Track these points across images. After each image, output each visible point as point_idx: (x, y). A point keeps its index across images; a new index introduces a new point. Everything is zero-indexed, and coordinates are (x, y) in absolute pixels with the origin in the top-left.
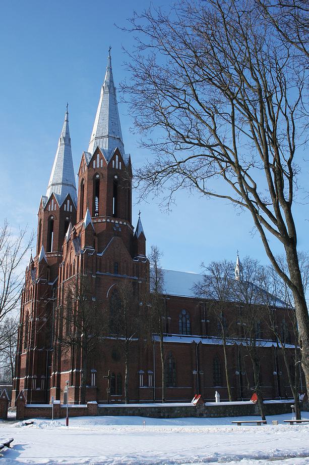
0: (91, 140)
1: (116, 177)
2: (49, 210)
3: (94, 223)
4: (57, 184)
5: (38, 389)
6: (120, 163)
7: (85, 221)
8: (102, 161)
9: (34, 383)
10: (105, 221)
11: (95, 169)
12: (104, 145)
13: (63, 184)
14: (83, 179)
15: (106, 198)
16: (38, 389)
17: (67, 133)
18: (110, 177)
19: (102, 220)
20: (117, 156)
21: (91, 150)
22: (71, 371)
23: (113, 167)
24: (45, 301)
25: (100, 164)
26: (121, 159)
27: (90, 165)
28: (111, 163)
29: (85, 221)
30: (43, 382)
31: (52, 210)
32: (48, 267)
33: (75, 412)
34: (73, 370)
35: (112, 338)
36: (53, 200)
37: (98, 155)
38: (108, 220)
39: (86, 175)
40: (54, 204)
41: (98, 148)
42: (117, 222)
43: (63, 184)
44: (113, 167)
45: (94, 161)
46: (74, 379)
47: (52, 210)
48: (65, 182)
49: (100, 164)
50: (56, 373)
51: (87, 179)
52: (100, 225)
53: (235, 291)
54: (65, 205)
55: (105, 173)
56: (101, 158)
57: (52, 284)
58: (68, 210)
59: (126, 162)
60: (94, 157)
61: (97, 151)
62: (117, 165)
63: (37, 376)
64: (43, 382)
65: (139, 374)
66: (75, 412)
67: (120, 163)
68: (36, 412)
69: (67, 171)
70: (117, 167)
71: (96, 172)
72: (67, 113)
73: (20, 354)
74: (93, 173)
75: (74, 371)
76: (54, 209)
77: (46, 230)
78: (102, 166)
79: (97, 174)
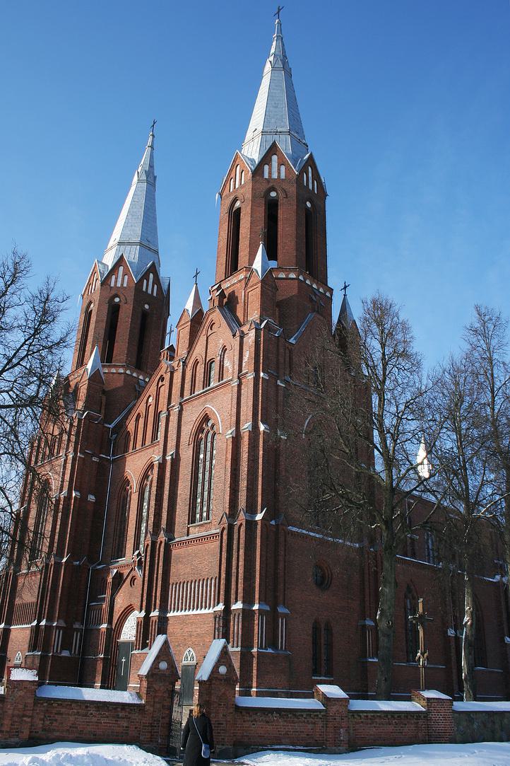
0: (109, 246)
1: (308, 204)
2: (112, 285)
3: (104, 373)
4: (130, 244)
5: (65, 654)
6: (156, 286)
7: (89, 366)
8: (126, 277)
9: (57, 638)
10: (122, 371)
11: (268, 181)
12: (132, 255)
13: (141, 244)
14: (91, 302)
15: (294, 236)
16: (65, 654)
17: (151, 166)
18: (300, 201)
19: (287, 275)
20: (151, 275)
21: (109, 260)
22: (35, 623)
23: (144, 289)
24: (95, 459)
25: (279, 173)
26: (157, 280)
27: (105, 282)
28: (140, 282)
29: (89, 366)
30: (76, 638)
31: (119, 285)
32: (104, 392)
33: (391, 728)
34: (39, 622)
35: (312, 534)
36: (121, 269)
37: (275, 158)
38: (128, 372)
39: (96, 298)
40: (124, 276)
41: (122, 257)
42: (141, 377)
43: (141, 244)
44: (144, 289)
45: (114, 277)
46: (38, 640)
47: (119, 285)
48: (145, 243)
49: (279, 173)
50: (43, 623)
51: (97, 303)
52: (284, 283)
53: (479, 470)
54: (145, 281)
55: (131, 296)
56: (282, 163)
57: (111, 426)
58: (150, 292)
59: (165, 287)
60: (266, 160)
61: (120, 261)
62: (149, 287)
63: (66, 622)
64: (76, 638)
65: (364, 626)
66: (391, 728)
67: (156, 286)
68: (269, 728)
69: (149, 225)
70: (150, 292)
71: (271, 184)
72: (153, 136)
73: (15, 572)
74: (264, 187)
75: (43, 623)
76: (122, 285)
77: (102, 321)
78: (125, 285)
79: (273, 189)
